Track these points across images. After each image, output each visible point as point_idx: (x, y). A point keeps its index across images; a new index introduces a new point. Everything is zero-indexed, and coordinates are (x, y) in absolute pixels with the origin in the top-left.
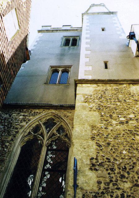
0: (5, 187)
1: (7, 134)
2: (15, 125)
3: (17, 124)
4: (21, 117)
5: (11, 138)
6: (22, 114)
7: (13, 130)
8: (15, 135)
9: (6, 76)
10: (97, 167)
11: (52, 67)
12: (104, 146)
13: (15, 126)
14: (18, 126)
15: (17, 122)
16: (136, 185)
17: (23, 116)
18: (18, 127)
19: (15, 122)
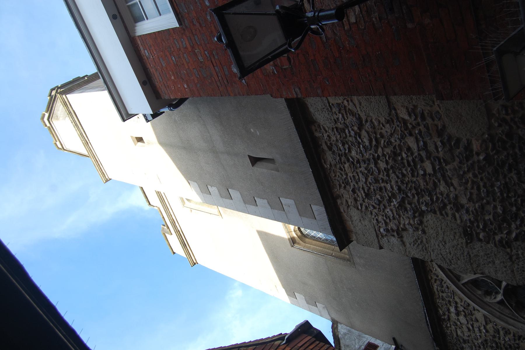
2: (487, 334)
4: (462, 318)
6: (453, 316)
7: (501, 338)
14: (490, 326)
18: (492, 329)
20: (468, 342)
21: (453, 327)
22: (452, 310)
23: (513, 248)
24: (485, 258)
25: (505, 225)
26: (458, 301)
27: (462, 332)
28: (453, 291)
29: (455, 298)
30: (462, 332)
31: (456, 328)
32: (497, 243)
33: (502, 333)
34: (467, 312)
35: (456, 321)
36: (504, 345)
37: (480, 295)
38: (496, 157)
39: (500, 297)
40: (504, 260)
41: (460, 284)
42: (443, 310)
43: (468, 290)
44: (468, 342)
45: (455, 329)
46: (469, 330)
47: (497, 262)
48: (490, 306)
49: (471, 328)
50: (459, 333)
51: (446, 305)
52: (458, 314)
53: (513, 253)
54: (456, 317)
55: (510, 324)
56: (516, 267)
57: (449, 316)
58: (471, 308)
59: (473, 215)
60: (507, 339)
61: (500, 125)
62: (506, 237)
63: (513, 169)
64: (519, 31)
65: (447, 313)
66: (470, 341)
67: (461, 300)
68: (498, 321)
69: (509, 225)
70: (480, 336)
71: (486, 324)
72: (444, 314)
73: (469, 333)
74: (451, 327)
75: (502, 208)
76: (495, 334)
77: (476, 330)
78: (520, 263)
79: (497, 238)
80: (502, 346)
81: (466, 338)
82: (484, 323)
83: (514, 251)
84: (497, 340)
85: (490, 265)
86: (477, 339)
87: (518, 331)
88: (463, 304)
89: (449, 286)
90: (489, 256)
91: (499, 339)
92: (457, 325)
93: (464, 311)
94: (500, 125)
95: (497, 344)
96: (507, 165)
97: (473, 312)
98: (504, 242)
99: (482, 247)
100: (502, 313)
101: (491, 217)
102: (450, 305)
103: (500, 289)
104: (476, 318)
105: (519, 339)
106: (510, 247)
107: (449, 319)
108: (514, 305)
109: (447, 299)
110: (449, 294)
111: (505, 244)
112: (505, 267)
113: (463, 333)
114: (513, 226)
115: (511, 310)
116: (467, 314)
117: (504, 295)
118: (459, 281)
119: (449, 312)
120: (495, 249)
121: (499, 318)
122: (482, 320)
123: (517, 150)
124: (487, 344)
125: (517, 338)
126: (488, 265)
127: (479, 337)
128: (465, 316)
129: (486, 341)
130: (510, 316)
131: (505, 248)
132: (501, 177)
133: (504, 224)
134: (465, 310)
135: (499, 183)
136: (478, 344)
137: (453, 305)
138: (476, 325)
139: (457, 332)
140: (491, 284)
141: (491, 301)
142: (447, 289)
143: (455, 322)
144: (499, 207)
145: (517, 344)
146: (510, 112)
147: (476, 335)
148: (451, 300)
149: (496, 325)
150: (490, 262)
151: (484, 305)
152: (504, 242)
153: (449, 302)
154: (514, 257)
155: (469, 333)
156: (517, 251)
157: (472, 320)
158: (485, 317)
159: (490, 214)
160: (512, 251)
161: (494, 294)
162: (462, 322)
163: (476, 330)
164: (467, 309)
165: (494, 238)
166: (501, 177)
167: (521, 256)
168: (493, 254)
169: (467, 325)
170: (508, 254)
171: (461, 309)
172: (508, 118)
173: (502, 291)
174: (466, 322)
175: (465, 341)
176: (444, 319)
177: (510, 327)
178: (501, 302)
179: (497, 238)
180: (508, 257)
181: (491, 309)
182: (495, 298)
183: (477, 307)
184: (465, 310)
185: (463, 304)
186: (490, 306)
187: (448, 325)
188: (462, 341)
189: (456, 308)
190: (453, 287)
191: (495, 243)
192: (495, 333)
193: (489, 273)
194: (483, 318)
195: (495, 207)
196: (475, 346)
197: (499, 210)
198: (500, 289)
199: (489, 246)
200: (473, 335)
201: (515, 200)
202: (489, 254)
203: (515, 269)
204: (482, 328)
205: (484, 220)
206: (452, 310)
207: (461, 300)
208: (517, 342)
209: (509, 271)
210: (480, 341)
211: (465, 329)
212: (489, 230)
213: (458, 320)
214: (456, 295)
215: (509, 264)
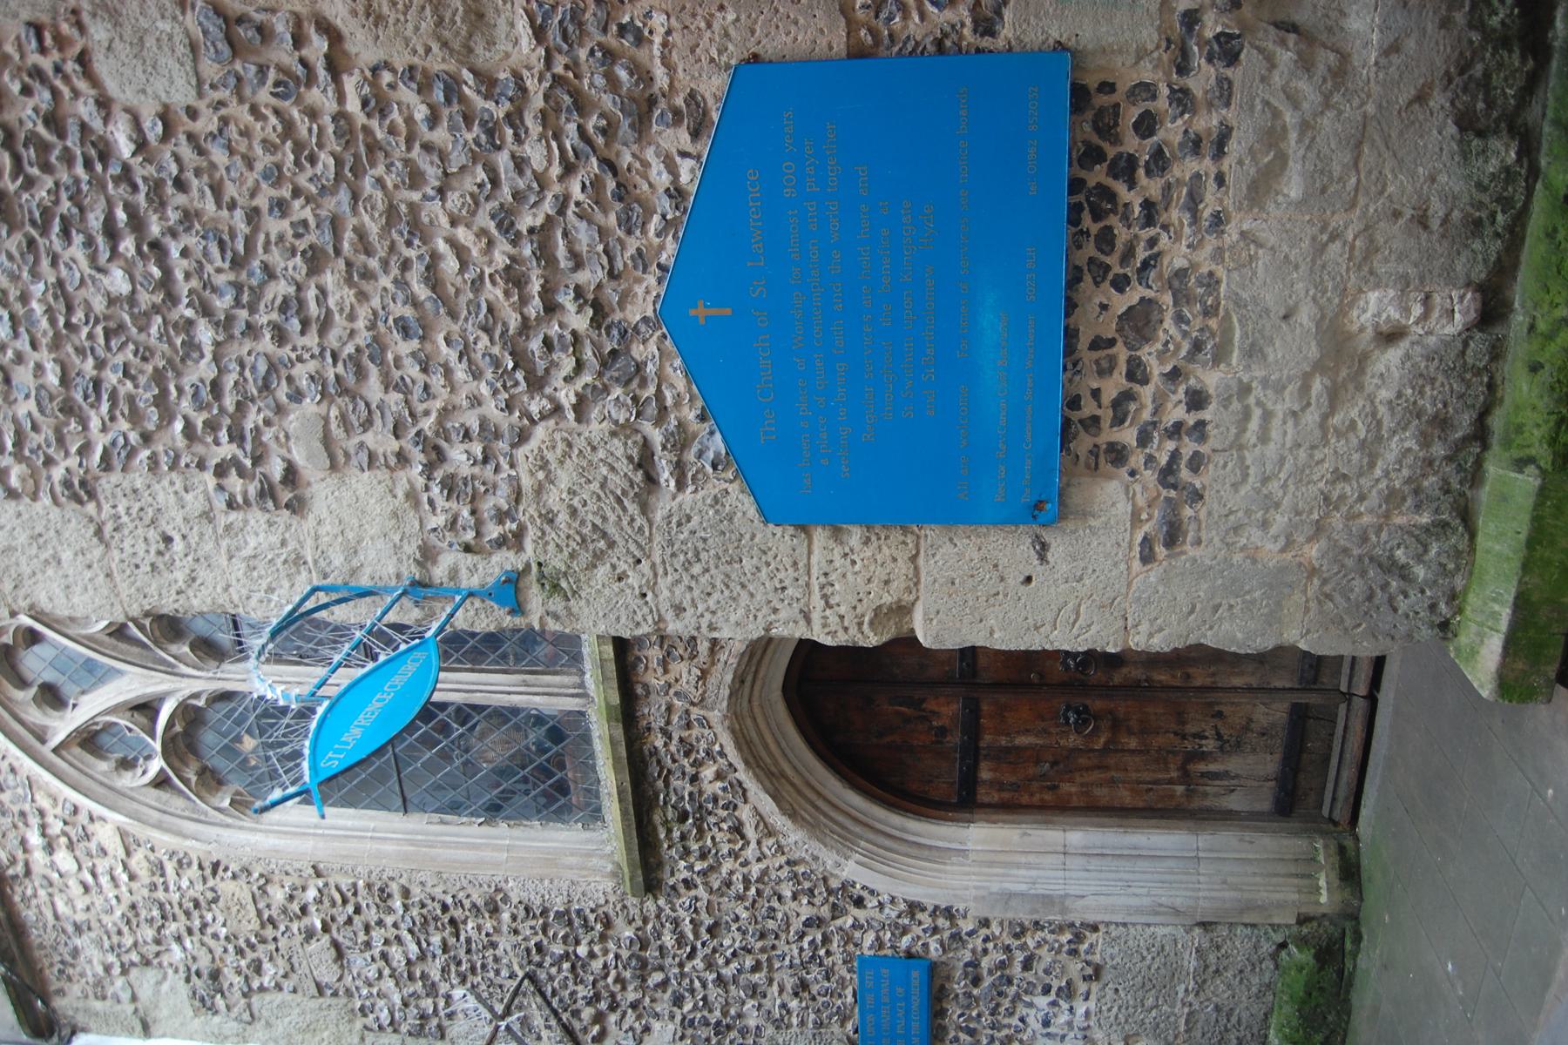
0: (511, 838)
1: (210, 910)
2: (135, 885)
3: (125, 877)
4: (64, 859)
5: (226, 887)
6: (39, 857)
7: (172, 887)
8: (207, 864)
9: (458, 845)
10: (276, 469)
11: (332, 457)
12: (113, 419)
13: (147, 881)
14: (138, 861)
15: (113, 878)
16: (1405, 5)
17: (50, 848)
18: (145, 864)
19: (117, 886)
20: (89, 929)
21: (42, 893)
22: (35, 839)
23: (103, 501)
24: (34, 551)
25: (73, 425)
26: (44, 803)
27: (70, 902)
28: (28, 778)
29: (37, 797)
30: (70, 902)
31: (50, 895)
32: (58, 489)
33: (170, 868)
34: (73, 834)
35: (48, 872)
36: (180, 905)
37: (104, 774)
38: (25, 196)
39: (157, 764)
40: (85, 545)
41: (46, 750)
42: (9, 846)
43: (71, 764)
44: (89, 929)
45: (47, 899)
46: (86, 889)
47: (66, 556)
48: (132, 799)
49: (89, 879)
50: (62, 907)
51: (15, 826)
52: (50, 848)
53: (103, 516)
54: (48, 859)
55: (185, 837)
56: (117, 560)
57: (27, 864)
58: (83, 818)
59: (20, 462)
60: (185, 883)
61: (26, 91)
62: (80, 465)
63: (74, 232)
64: (1324, 788)
65: (20, 855)
66: (94, 924)
67: (55, 800)
68: (157, 836)
69: (84, 423)
70: (117, 897)
71: (128, 853)
72: (13, 861)
73: (87, 900)
74: (35, 896)
75: (58, 369)
76: (155, 879)
77: (104, 880)
78: (126, 545)
79: (58, 473)
80: (177, 909)
81: (80, 917)
82: (121, 853)
83: (106, 507)
84: (160, 895)
85: (50, 572)
86: (111, 911)
87: (209, 848)
88: (58, 811)
89: (16, 764)
90: (41, 541)
91: (166, 890)
92: (51, 885)
93: (65, 834)
94: (26, 91)
95: (161, 906)
96: (57, 220)
97: (91, 828)
98: (76, 483)
99: (19, 515)
100: (165, 812)
101: (31, 405)
102: (27, 825)
103: (153, 737)
104: (99, 844)
105: (214, 873)
106: (92, 495)
107: (28, 873)
108: (194, 779)
109: (16, 809)
110: (20, 791)
111: (82, 491)
112: (89, 567)
113: (71, 905)
114: (95, 423)
115: (189, 799)
116: (75, 839)
117: (166, 754)
118: (43, 741)
119: (25, 851)
120: (55, 513)
121: (159, 826)
122: (115, 846)
123: (80, 170)
124: (137, 915)
125: (208, 871)
126: (44, 572)
127: (114, 902)
128: (71, 846)
129: (133, 907)
130: (187, 813)
131: (80, 502)
132: (45, 263)
133: (68, 424)
134: (67, 828)
135: (41, 286)
136: (115, 924)
137: (34, 821)
138: (102, 866)
139: (53, 904)
140: (130, 730)
141: (135, 785)
142: (11, 777)
143: (45, 877)
144: (49, 366)
145: (213, 890)
146: (48, 41)
147: (106, 900)
148: (27, 807)
149: (152, 849)
150: (47, 562)
151: (112, 798)
152: (76, 483)
153: (23, 814)
154: (108, 529)
155: (87, 900)
156: (114, 507)
157: (90, 855)
158: (123, 834)
159: (27, 396)
160: (99, 507)
161: (141, 761)
162: (63, 871)
163: (104, 880)
164: (74, 825)
165: (49, 478)
166: (45, 263)
167: (125, 519)
168: (52, 533)
169: (80, 876)
170: (91, 520)
171: (56, 827)
172: (46, 64)
173: (157, 746)
174: (75, 866)
175: (78, 929)
176: (17, 876)
177: (189, 843)
178: (161, 782)
179: (58, 473)
180: (92, 529)
181: (135, 806)
182: (144, 773)
183: (98, 809)
184: (67, 828)
185: (58, 811)
186: (132, 799)
187: (29, 892)
188: (70, 929)
189: (43, 827)
190: (27, 765)
191: (52, 491)
192: (153, 874)
193: (51, 599)
194: (118, 839)
195: (39, 369)
196: (107, 933)
197: (52, 379)
198: (153, 737)
199: (38, 506)
200: (99, 902)
201: (91, 336)
202: (40, 535)
203: (114, 566)
204: (119, 870)
205: (15, 420)
206: (35, 839)
207: (55, 800)
208: (211, 883)
209: (102, 577)
210: (118, 913)
211: (76, 890)
212: (32, 451)
213: (53, 865)
214: (40, 788)
215: (98, 551)
